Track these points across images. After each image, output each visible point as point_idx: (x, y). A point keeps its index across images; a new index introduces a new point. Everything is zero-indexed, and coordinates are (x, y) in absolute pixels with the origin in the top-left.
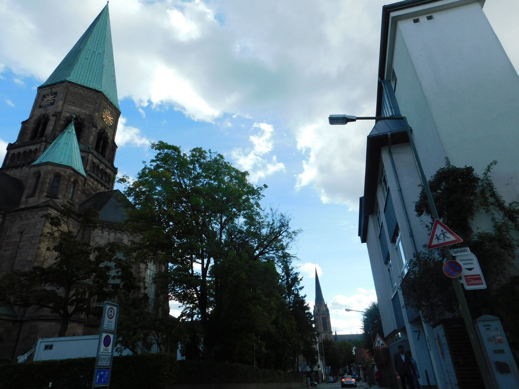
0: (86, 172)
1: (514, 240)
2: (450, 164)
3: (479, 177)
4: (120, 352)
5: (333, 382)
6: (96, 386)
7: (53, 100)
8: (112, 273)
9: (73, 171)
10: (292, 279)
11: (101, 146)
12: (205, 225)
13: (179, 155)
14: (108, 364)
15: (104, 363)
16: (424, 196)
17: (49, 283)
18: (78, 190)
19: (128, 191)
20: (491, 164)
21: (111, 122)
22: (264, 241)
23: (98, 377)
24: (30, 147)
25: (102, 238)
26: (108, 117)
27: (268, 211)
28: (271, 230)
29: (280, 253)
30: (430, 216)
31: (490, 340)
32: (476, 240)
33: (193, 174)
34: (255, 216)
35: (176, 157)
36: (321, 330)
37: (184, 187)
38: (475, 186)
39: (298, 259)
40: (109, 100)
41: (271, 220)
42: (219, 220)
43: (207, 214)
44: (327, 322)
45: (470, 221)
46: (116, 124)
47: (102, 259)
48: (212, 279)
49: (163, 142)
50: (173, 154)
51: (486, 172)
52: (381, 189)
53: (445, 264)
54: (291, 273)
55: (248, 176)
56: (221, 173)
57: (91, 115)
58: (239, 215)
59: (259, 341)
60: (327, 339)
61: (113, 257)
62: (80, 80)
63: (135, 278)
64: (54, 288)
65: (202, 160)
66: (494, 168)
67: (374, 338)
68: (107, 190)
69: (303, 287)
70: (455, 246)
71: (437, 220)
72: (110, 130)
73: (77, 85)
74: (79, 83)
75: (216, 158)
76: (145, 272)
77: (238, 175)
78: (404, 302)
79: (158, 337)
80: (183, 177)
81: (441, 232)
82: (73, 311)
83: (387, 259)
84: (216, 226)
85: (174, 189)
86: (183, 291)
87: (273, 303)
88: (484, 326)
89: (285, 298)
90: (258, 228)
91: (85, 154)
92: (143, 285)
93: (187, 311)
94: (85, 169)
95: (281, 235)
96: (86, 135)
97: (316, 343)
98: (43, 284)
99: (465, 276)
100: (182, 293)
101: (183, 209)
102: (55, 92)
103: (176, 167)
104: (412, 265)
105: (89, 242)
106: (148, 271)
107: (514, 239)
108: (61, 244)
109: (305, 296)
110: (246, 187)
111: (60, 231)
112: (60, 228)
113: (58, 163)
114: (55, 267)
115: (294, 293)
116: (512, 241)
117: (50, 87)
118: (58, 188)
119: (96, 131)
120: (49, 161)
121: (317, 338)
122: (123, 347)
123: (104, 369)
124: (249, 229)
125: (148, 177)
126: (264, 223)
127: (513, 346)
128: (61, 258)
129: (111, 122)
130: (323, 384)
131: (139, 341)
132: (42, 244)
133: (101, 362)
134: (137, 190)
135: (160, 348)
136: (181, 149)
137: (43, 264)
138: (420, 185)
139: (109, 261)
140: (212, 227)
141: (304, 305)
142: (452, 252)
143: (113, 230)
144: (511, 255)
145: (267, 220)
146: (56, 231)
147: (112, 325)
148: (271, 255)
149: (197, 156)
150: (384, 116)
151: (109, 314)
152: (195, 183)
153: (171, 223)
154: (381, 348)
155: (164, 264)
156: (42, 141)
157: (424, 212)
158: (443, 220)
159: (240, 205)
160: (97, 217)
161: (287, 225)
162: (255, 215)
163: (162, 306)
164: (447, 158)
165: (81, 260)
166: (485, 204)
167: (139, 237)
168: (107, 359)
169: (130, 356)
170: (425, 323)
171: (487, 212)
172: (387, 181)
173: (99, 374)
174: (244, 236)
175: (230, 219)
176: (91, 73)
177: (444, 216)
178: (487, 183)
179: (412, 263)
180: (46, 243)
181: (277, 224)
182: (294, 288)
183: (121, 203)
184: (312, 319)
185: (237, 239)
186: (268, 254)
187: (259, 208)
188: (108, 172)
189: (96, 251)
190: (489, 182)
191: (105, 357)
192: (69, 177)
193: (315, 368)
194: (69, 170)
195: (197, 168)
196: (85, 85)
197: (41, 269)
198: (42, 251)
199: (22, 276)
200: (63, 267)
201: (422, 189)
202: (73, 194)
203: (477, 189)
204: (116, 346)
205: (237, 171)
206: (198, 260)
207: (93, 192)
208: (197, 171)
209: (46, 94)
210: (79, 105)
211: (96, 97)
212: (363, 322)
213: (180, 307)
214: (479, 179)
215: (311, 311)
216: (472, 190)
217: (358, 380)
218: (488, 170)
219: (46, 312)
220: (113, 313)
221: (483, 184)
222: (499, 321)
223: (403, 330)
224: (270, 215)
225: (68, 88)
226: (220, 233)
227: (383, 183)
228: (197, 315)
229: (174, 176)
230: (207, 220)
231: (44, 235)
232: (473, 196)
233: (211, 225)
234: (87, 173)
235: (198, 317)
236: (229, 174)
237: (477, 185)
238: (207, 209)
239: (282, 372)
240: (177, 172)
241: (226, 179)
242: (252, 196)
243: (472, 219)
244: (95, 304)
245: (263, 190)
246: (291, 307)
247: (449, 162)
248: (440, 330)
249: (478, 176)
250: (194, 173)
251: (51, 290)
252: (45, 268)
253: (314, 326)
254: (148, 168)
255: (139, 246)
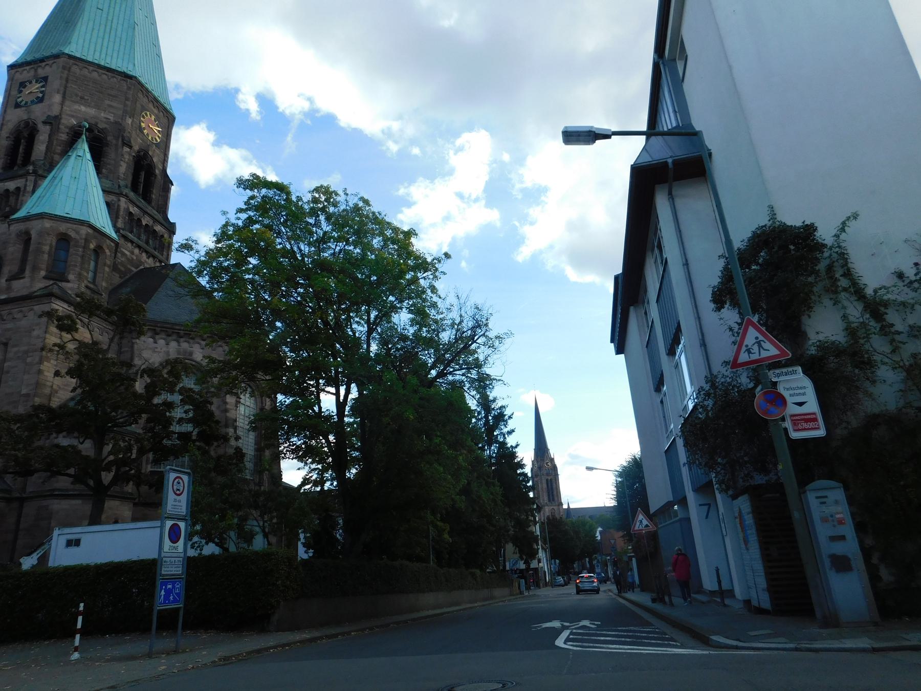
0: (117, 230)
1: (878, 353)
2: (776, 218)
3: (825, 242)
4: (199, 549)
5: (563, 586)
6: (161, 608)
7: (42, 92)
8: (177, 412)
9: (93, 231)
10: (494, 417)
11: (141, 183)
12: (340, 326)
13: (288, 200)
14: (179, 571)
15: (171, 569)
16: (727, 276)
17: (64, 433)
18: (105, 264)
19: (196, 266)
20: (848, 218)
21: (158, 136)
22: (445, 354)
23: (163, 593)
24: (6, 184)
25: (154, 352)
26: (151, 126)
27: (452, 299)
28: (457, 333)
29: (474, 374)
30: (737, 311)
31: (824, 520)
32: (813, 352)
33: (315, 235)
34: (429, 310)
35: (283, 203)
36: (544, 500)
37: (299, 258)
38: (817, 259)
39: (505, 384)
40: (151, 92)
41: (458, 316)
42: (364, 317)
43: (343, 307)
44: (554, 487)
45: (804, 319)
46: (167, 139)
47: (157, 389)
48: (354, 420)
49: (258, 176)
50: (277, 197)
51: (839, 233)
52: (653, 261)
53: (759, 397)
54: (493, 407)
55: (415, 236)
56: (366, 232)
57: (119, 122)
58: (401, 308)
59: (439, 524)
60: (553, 516)
61: (176, 385)
62: (91, 52)
63: (218, 422)
64: (75, 442)
65: (331, 209)
66: (853, 226)
67: (634, 515)
68: (158, 264)
69: (513, 431)
70: (776, 364)
71: (748, 319)
72: (157, 151)
73: (86, 62)
74: (90, 59)
75: (356, 205)
76: (236, 410)
77: (397, 236)
78: (687, 458)
79: (264, 522)
80: (297, 239)
81: (755, 341)
82: (111, 480)
83: (659, 384)
84: (361, 328)
85: (282, 262)
86: (305, 443)
87: (461, 459)
88: (817, 498)
89: (483, 449)
90: (434, 330)
91: (112, 198)
92: (233, 432)
93: (312, 477)
94: (114, 226)
95: (475, 342)
96: (113, 162)
97: (535, 523)
98: (54, 435)
99: (792, 416)
100: (303, 446)
101: (299, 299)
102: (43, 75)
103: (283, 221)
104: (702, 396)
105: (132, 359)
106: (242, 409)
107: (878, 351)
108: (80, 365)
109: (517, 446)
110: (412, 258)
111: (76, 340)
112: (77, 336)
113: (62, 215)
114: (72, 404)
115: (498, 441)
116: (874, 355)
117: (32, 66)
118: (66, 262)
119: (130, 154)
120: (47, 212)
121: (536, 514)
122: (204, 541)
123: (173, 579)
124: (418, 332)
125: (232, 241)
126: (446, 322)
127: (860, 528)
128: (82, 390)
129: (158, 136)
130: (547, 588)
131: (231, 530)
132: (45, 363)
133: (165, 569)
134: (214, 264)
135: (268, 540)
136: (292, 189)
137: (50, 400)
138: (722, 256)
139: (170, 393)
140: (352, 330)
141: (516, 461)
142: (772, 375)
143: (174, 337)
144: (871, 379)
145: (450, 316)
146: (69, 341)
147: (181, 506)
148: (458, 377)
149: (321, 201)
150: (662, 130)
151: (175, 487)
152: (319, 251)
153: (278, 324)
154: (644, 532)
155: (269, 397)
156: (28, 173)
157: (726, 304)
158: (759, 317)
159: (403, 290)
160: (143, 316)
161: (486, 325)
162: (428, 307)
163: (267, 470)
164: (771, 207)
165: (119, 392)
166: (833, 290)
167: (221, 349)
168: (176, 563)
169: (217, 555)
170: (720, 493)
171: (834, 304)
172: (664, 247)
173: (164, 587)
174: (409, 346)
175: (384, 315)
176: (112, 39)
177: (761, 310)
178: (839, 252)
179: (702, 393)
180: (52, 361)
181: (468, 324)
182: (498, 433)
183: (187, 290)
184: (528, 485)
185: (398, 350)
186: (452, 376)
187: (435, 295)
188: (159, 230)
189: (145, 376)
190: (843, 251)
191: (173, 559)
192: (85, 242)
193: (534, 564)
194: (85, 227)
195: (322, 222)
196: (102, 63)
197: (50, 410)
198: (46, 376)
199: (13, 423)
200: (87, 405)
201: (725, 262)
202: (95, 273)
203: (822, 263)
204: (191, 540)
205: (396, 230)
206: (329, 389)
207: (133, 269)
208: (322, 229)
209: (26, 80)
210: (93, 103)
211: (126, 88)
212: (615, 487)
213: (299, 469)
214: (824, 246)
215: (528, 470)
216: (812, 265)
217: (603, 581)
218: (843, 230)
219: (63, 482)
220: (182, 485)
221: (831, 255)
222: (842, 489)
223: (683, 502)
224: (456, 307)
225: (70, 68)
226: (367, 339)
227: (656, 251)
228: (330, 482)
229: (281, 239)
230: (343, 317)
231: (48, 347)
232: (813, 275)
233: (351, 325)
234: (119, 232)
235: (332, 484)
236: (381, 234)
237: (821, 256)
238: (342, 298)
239: (478, 572)
240: (287, 232)
241: (376, 242)
242: (423, 274)
243: (809, 317)
244: (149, 466)
245: (442, 262)
246: (493, 464)
247: (775, 214)
248: (744, 504)
249: (824, 240)
250: (316, 233)
251: (69, 445)
252: (54, 406)
253: (531, 495)
254: (233, 225)
255: (222, 365)
